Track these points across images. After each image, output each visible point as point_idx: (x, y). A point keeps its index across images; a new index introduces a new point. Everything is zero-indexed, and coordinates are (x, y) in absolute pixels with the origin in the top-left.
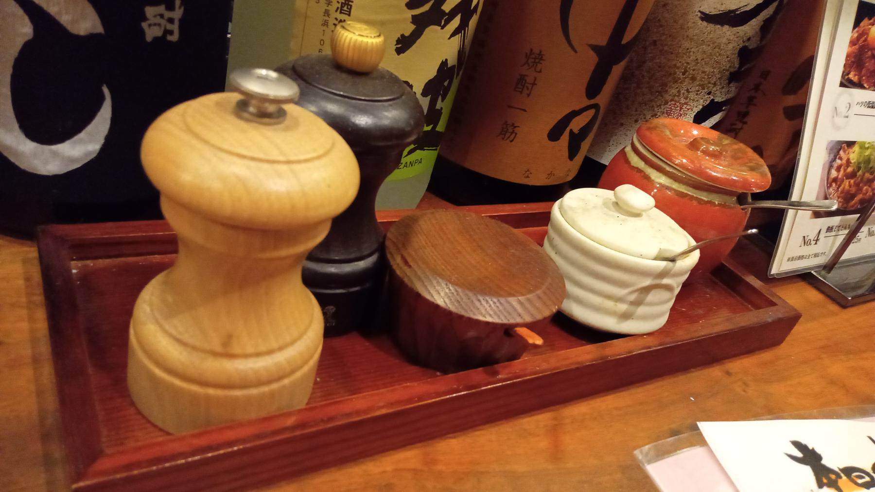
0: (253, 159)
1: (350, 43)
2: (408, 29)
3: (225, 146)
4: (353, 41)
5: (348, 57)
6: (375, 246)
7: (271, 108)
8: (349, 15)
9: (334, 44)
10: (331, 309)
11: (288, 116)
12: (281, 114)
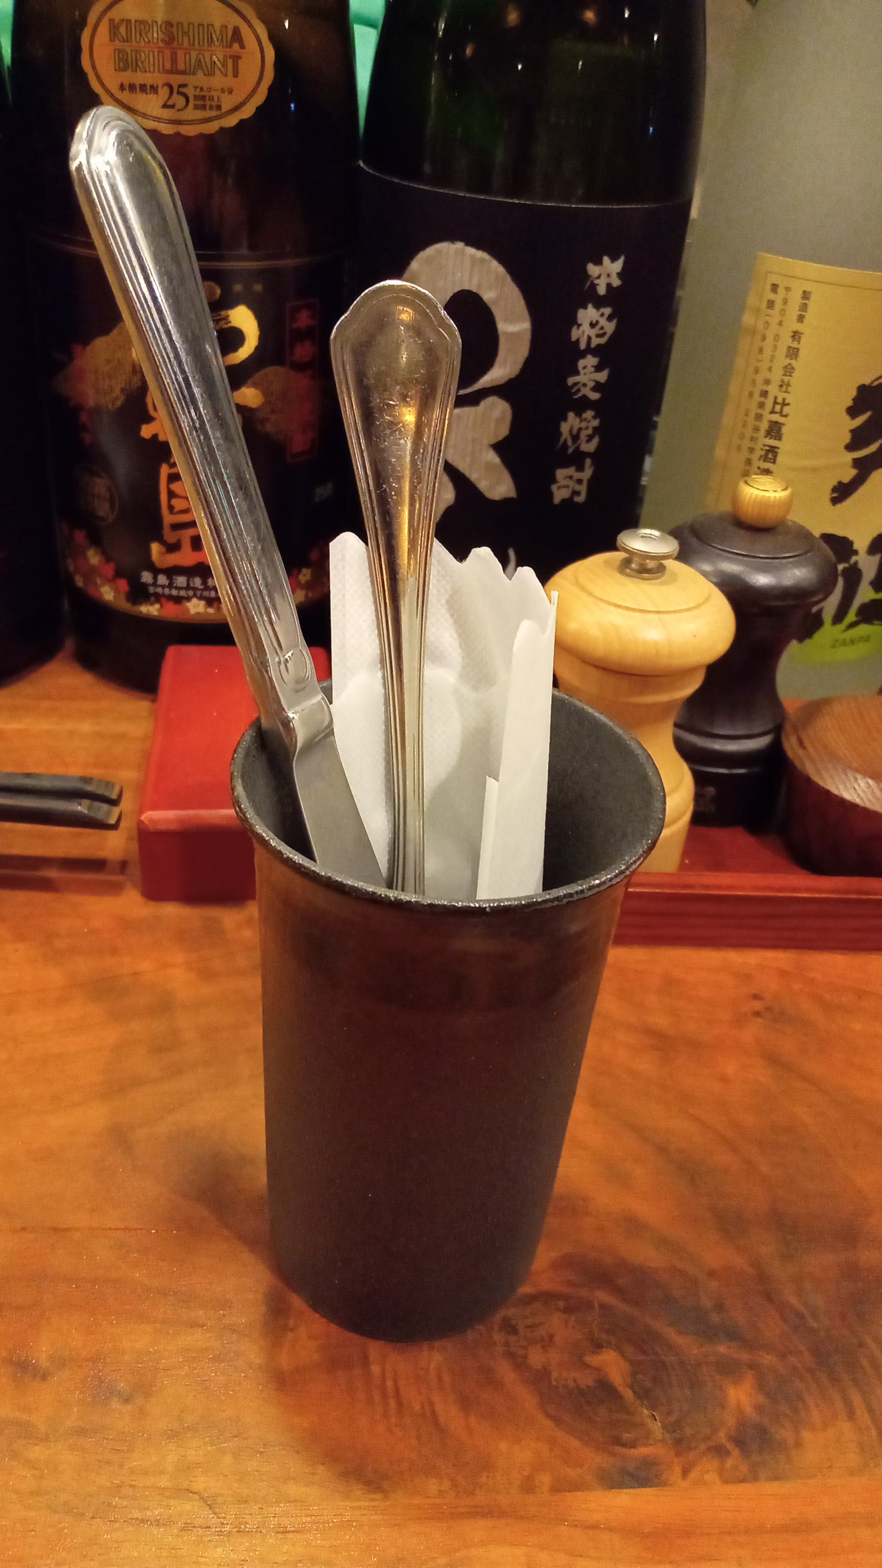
0: (628, 609)
1: (751, 497)
2: (848, 474)
3: (605, 598)
4: (754, 496)
5: (749, 513)
6: (770, 726)
7: (651, 564)
8: (774, 463)
9: (735, 500)
10: (711, 790)
11: (667, 572)
12: (661, 569)
